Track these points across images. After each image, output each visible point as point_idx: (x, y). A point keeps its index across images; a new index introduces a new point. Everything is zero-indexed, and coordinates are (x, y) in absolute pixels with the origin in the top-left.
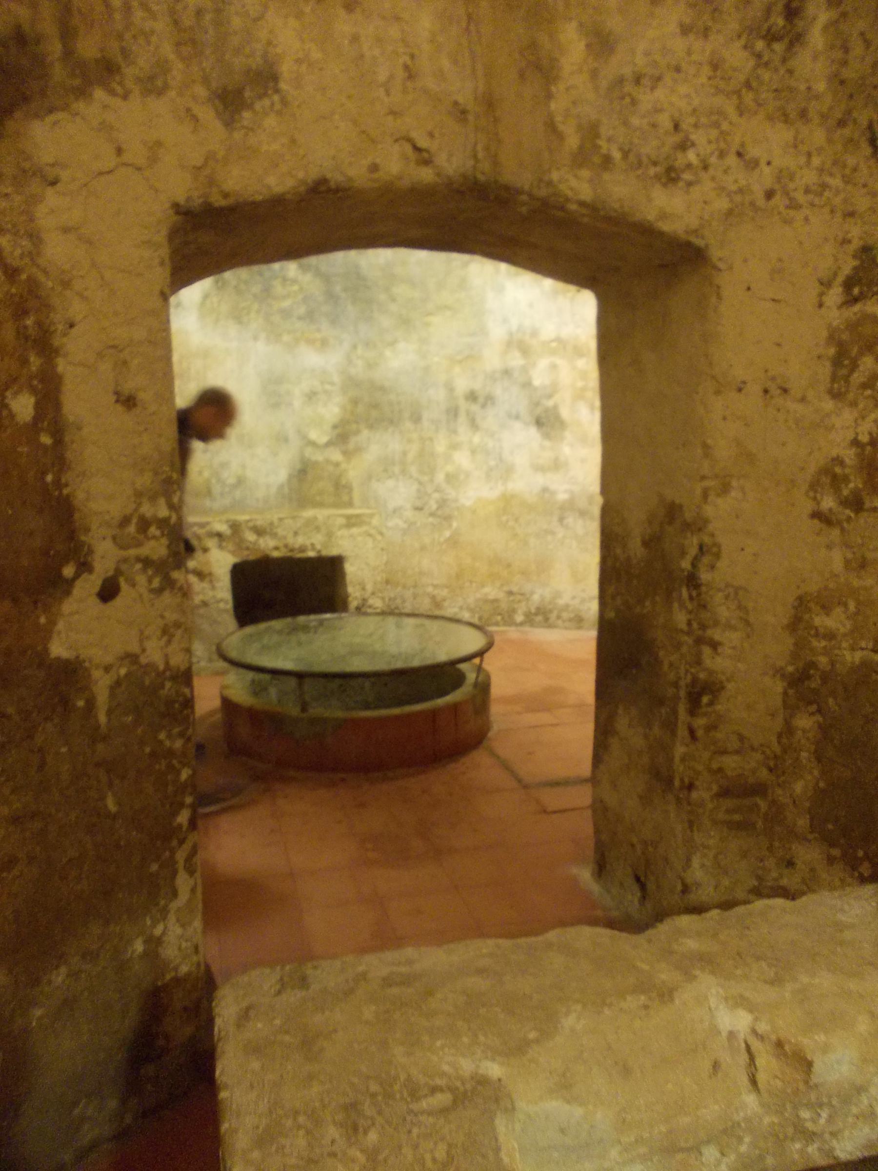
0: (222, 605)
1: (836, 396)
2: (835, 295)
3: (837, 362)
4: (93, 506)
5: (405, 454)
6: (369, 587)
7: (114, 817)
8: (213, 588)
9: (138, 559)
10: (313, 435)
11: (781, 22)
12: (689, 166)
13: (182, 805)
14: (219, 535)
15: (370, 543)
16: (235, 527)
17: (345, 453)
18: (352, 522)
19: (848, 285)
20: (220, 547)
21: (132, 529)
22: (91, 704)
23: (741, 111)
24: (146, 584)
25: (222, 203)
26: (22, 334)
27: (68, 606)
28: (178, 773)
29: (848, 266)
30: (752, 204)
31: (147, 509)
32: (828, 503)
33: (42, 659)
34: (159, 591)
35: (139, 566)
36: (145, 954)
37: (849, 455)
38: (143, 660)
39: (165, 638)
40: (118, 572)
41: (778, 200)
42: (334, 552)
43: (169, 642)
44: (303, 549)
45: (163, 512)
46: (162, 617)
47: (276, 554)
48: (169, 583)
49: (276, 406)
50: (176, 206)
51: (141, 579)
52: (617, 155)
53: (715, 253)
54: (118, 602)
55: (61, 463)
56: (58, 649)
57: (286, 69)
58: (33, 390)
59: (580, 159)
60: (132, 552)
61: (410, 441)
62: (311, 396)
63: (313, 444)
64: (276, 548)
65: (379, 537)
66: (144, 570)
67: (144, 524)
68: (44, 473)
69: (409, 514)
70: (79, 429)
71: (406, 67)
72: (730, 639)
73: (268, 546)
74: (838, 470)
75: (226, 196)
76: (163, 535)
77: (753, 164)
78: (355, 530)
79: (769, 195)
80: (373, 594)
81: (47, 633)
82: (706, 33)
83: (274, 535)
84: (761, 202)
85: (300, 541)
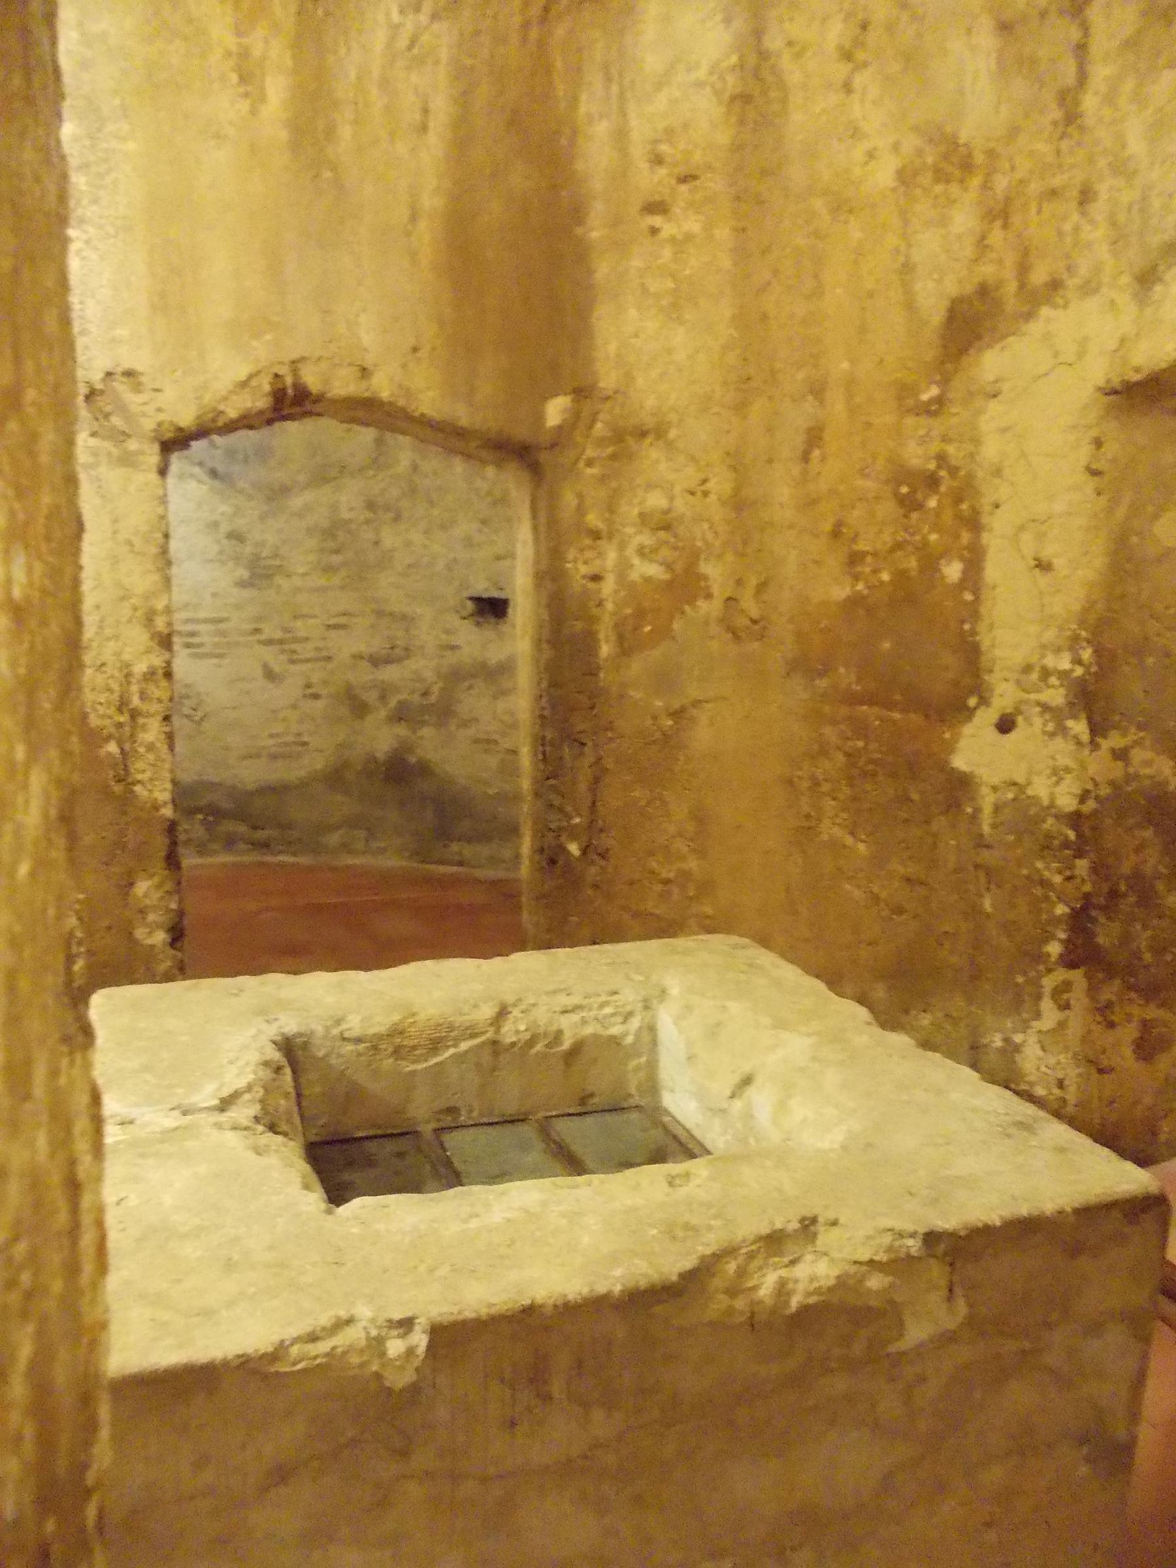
4: (997, 652)
7: (988, 916)
9: (1038, 704)
13: (1053, 937)
21: (1035, 676)
22: (978, 810)
24: (1041, 727)
26: (958, 517)
27: (967, 730)
28: (1054, 905)
31: (1050, 661)
33: (943, 767)
34: (1052, 735)
35: (1038, 709)
36: (1002, 1051)
38: (1030, 792)
39: (1054, 778)
40: (1018, 711)
43: (1057, 783)
46: (1053, 758)
51: (1038, 721)
54: (1013, 736)
55: (975, 615)
56: (959, 762)
58: (962, 558)
66: (1042, 713)
67: (1046, 673)
68: (963, 622)
70: (994, 588)
75: (1137, 370)
76: (1062, 685)
81: (950, 748)
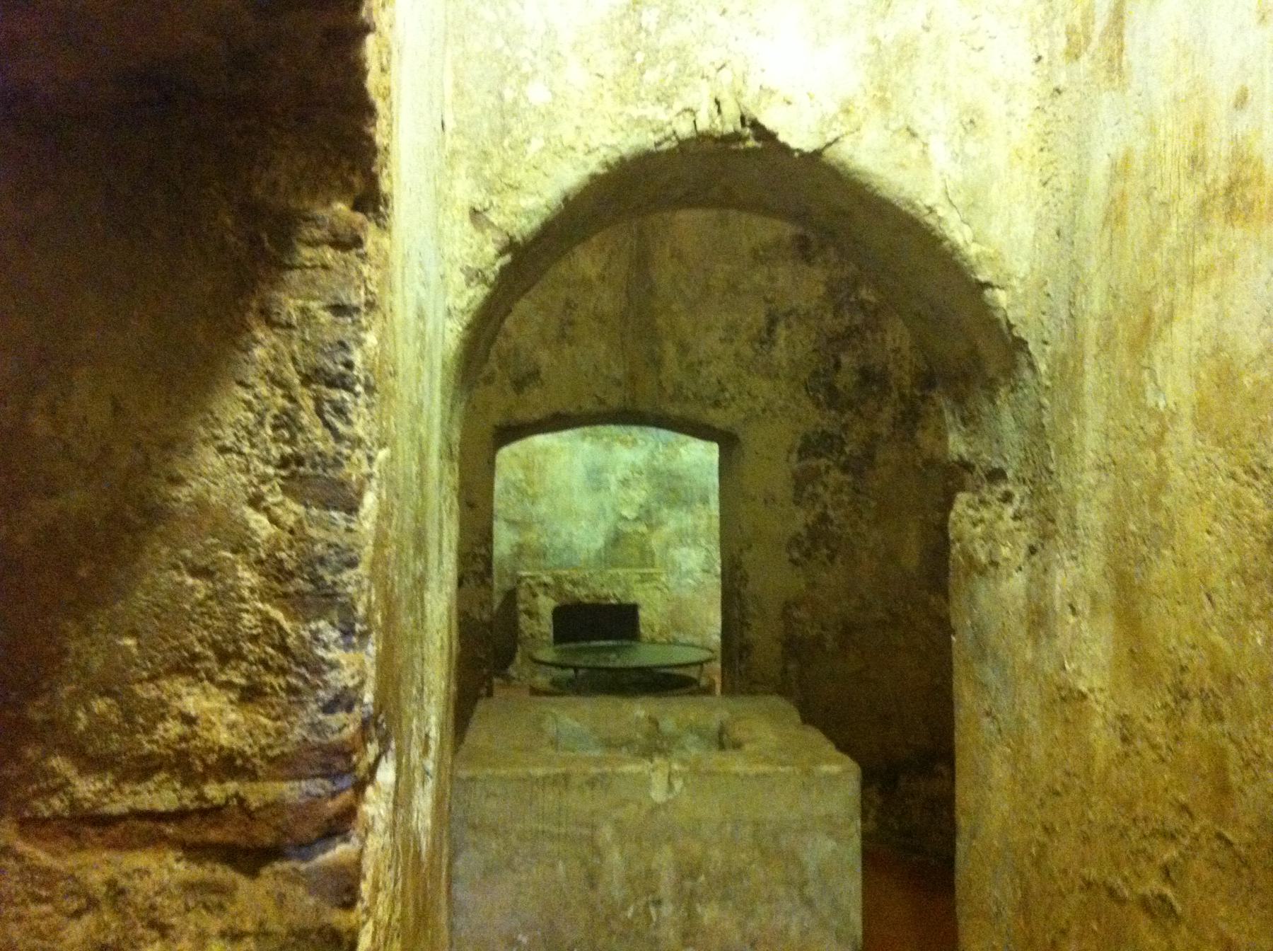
0: (545, 638)
1: (797, 503)
2: (794, 457)
3: (796, 488)
5: (696, 527)
6: (657, 629)
8: (539, 625)
10: (625, 513)
11: (765, 336)
12: (726, 399)
14: (545, 585)
15: (658, 594)
16: (557, 579)
17: (649, 526)
18: (644, 579)
19: (800, 452)
20: (546, 594)
23: (749, 373)
25: (514, 424)
29: (799, 443)
30: (757, 416)
31: (477, 550)
32: (796, 555)
37: (804, 532)
41: (768, 414)
42: (632, 600)
44: (607, 598)
45: (483, 551)
47: (586, 601)
48: (483, 582)
49: (598, 490)
50: (496, 427)
52: (692, 396)
53: (741, 437)
57: (544, 370)
59: (672, 399)
60: (470, 569)
61: (700, 517)
62: (625, 483)
63: (625, 519)
64: (587, 596)
65: (666, 590)
67: (475, 556)
69: (699, 575)
71: (595, 366)
72: (755, 623)
73: (581, 593)
74: (799, 538)
77: (755, 398)
78: (647, 585)
79: (764, 411)
80: (660, 634)
82: (732, 341)
83: (586, 586)
84: (760, 413)
85: (605, 591)
